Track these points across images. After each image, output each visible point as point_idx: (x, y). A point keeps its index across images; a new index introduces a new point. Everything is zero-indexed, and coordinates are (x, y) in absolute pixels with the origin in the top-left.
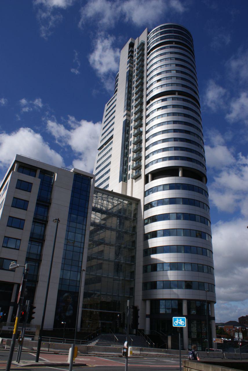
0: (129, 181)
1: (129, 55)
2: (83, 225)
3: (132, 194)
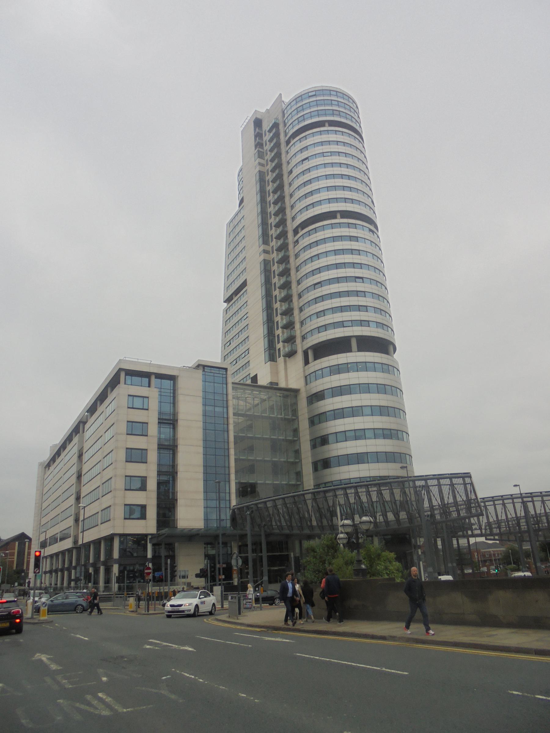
0: (281, 360)
1: (255, 141)
2: (226, 493)
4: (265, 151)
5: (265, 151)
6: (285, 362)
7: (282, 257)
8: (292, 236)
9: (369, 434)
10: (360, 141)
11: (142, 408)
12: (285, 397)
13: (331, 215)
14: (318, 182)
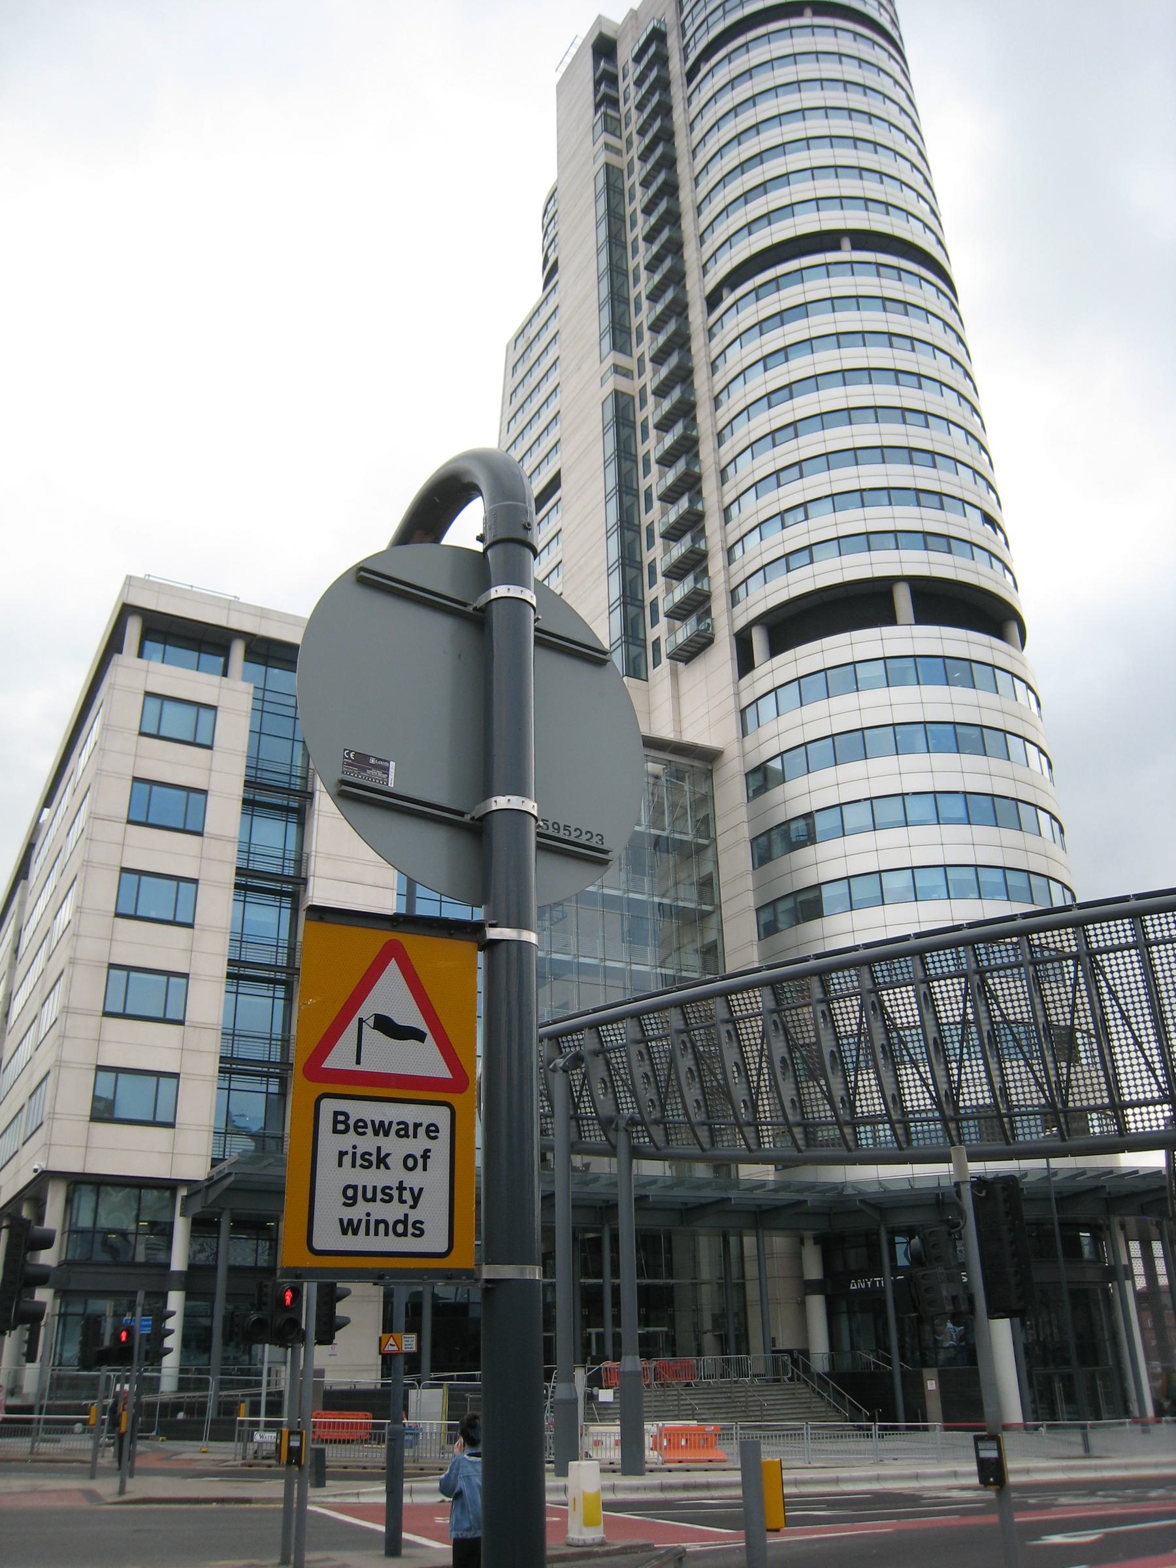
3: (678, 720)
4: (623, 116)
5: (623, 116)
6: (675, 675)
7: (687, 599)
8: (702, 312)
9: (903, 598)
10: (891, 56)
11: (190, 739)
12: (678, 775)
13: (825, 241)
14: (787, 188)
